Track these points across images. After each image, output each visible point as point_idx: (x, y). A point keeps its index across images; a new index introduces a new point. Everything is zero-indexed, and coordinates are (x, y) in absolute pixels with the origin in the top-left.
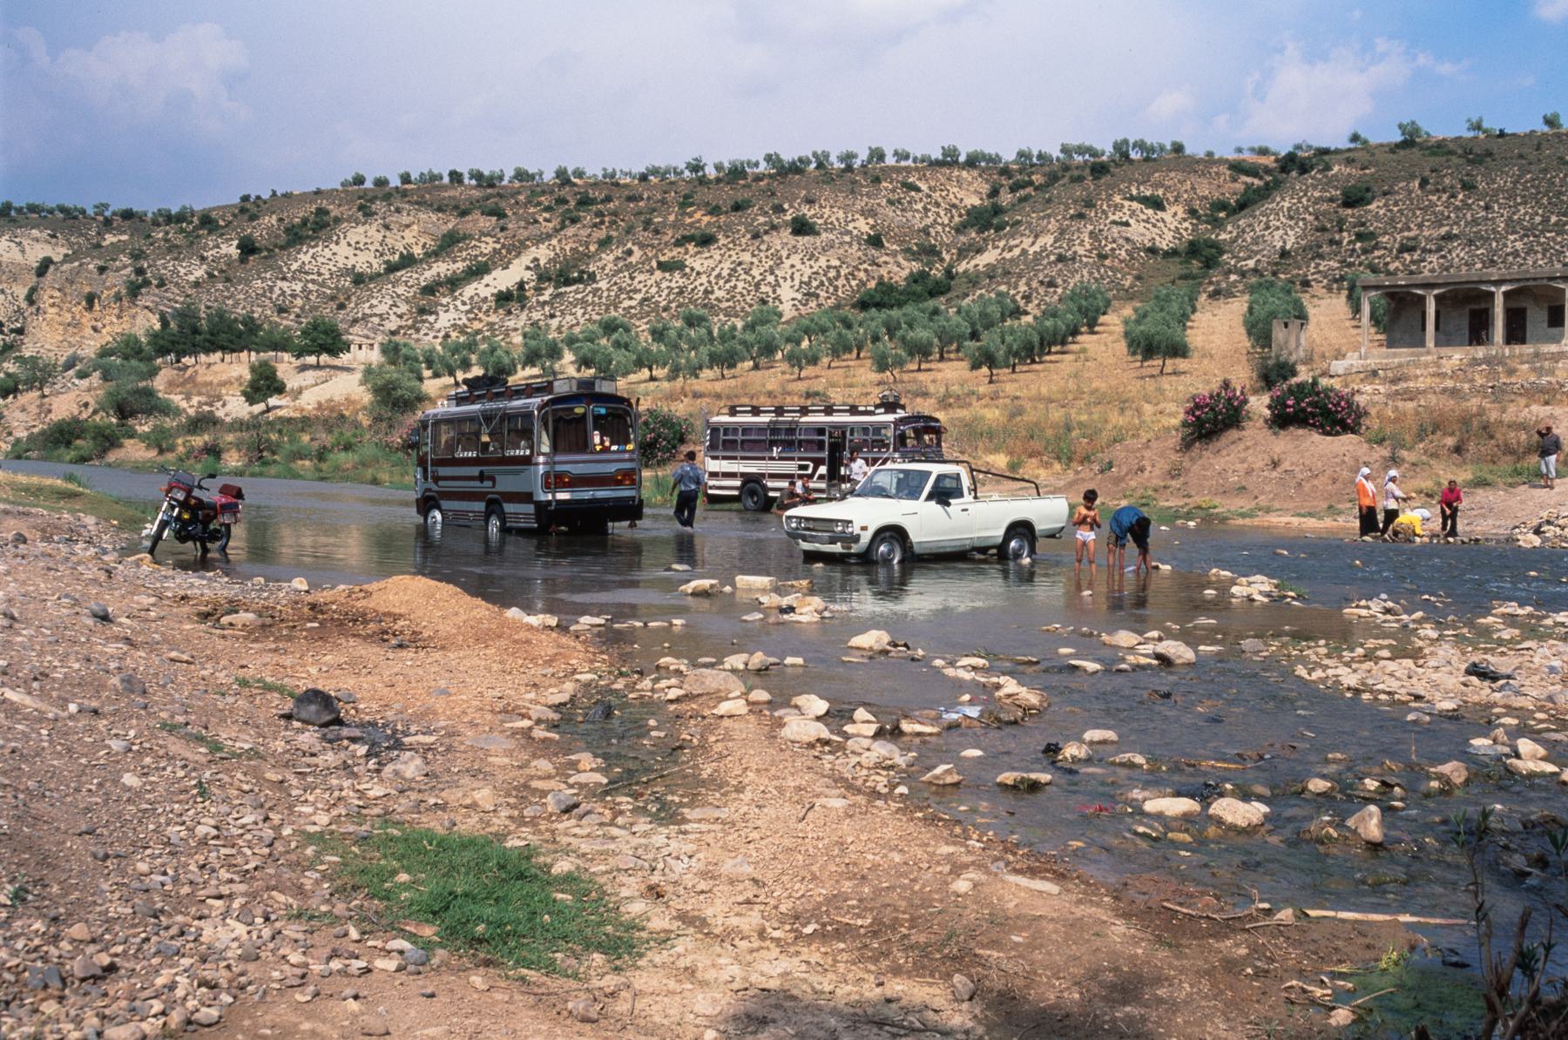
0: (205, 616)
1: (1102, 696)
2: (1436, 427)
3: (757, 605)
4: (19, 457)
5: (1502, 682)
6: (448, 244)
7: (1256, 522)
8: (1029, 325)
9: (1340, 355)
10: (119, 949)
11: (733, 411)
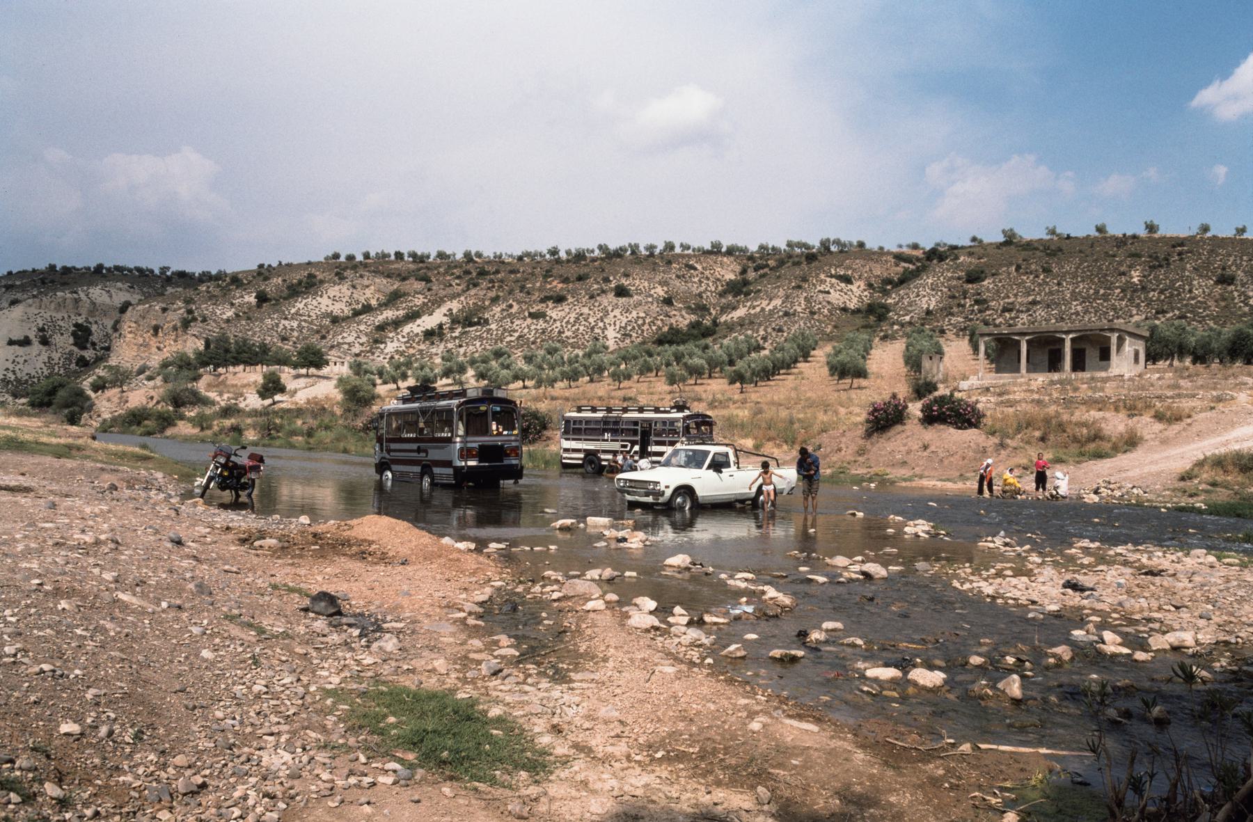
0: (243, 541)
2: (1028, 425)
3: (601, 537)
4: (105, 431)
5: (1087, 593)
6: (393, 299)
7: (914, 484)
8: (766, 357)
9: (965, 378)
10: (207, 772)
11: (579, 410)
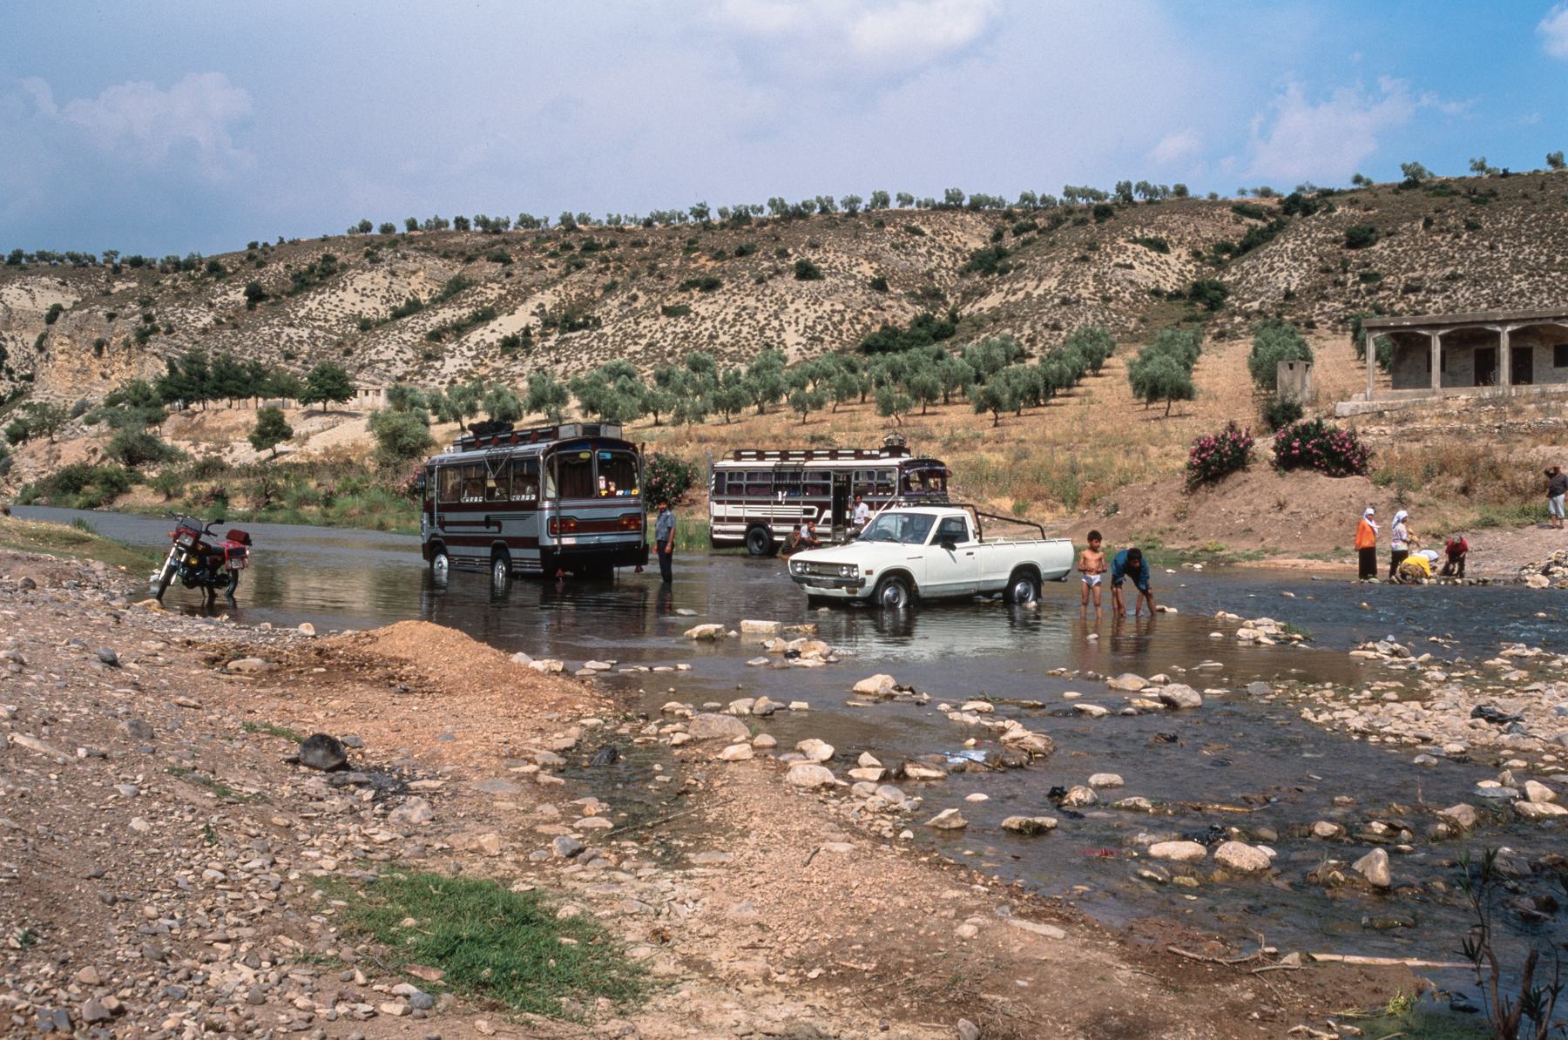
0: (212, 661)
1: (1110, 741)
2: (1443, 468)
3: (762, 650)
4: (28, 503)
6: (454, 290)
7: (1262, 564)
8: (1034, 368)
9: (1345, 396)
10: (128, 992)
11: (738, 456)
